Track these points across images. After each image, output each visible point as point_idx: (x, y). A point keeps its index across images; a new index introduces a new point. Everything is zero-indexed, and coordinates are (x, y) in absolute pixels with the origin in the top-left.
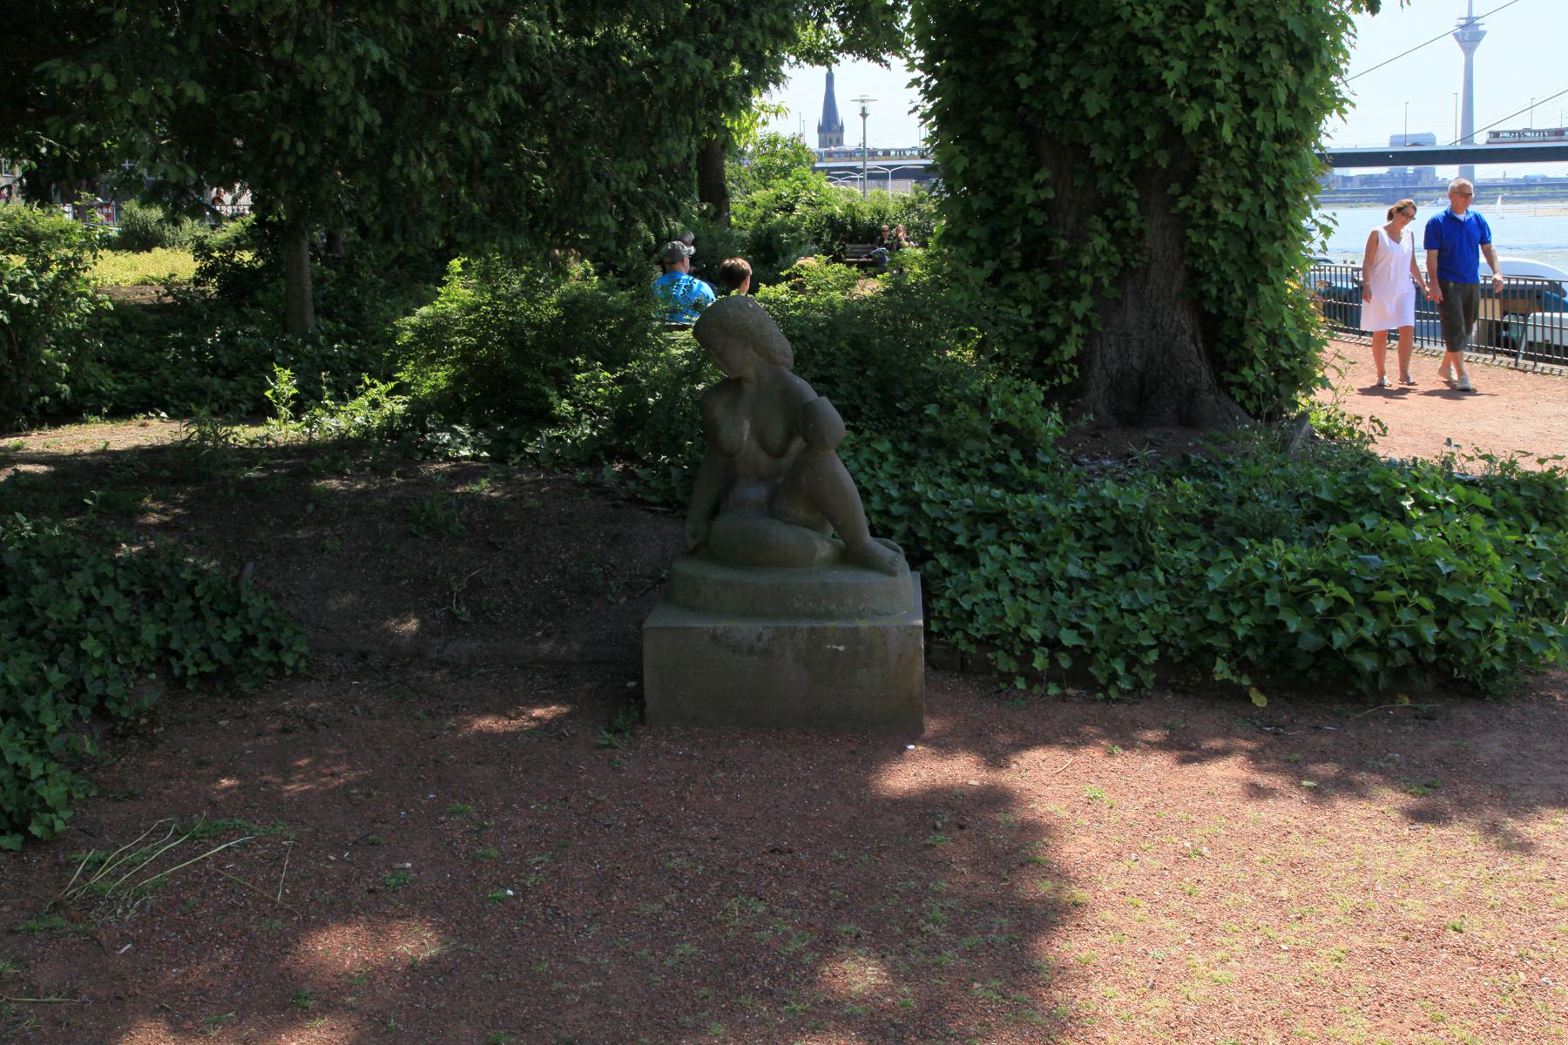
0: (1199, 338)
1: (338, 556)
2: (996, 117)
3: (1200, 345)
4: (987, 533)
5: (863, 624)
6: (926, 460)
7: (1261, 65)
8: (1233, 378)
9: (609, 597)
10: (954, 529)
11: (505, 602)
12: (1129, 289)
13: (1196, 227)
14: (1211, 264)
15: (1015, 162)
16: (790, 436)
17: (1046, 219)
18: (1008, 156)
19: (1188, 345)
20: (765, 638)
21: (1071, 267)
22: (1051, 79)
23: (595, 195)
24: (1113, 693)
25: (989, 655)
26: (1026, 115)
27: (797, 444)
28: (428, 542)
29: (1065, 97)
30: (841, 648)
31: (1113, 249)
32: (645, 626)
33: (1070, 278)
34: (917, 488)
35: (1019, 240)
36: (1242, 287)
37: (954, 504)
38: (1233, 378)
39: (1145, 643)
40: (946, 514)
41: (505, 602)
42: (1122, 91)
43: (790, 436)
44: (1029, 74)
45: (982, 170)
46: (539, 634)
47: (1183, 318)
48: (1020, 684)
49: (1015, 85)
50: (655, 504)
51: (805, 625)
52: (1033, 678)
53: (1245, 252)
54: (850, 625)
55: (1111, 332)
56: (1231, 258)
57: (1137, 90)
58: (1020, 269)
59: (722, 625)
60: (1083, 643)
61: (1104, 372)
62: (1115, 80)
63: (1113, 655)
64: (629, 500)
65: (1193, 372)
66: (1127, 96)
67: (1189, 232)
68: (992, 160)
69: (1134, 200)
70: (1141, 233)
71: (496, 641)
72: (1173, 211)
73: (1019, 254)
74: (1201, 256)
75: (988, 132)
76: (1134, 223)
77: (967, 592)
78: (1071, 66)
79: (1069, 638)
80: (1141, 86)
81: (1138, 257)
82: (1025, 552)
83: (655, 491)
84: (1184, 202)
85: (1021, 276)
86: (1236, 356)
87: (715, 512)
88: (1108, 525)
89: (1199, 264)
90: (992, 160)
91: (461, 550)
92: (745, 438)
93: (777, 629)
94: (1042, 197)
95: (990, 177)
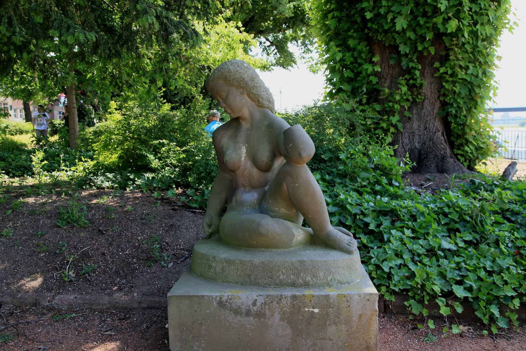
0: (445, 133)
1: (9, 239)
2: (355, 35)
3: (445, 137)
4: (386, 222)
5: (332, 292)
6: (339, 184)
7: (480, 4)
8: (460, 152)
9: (163, 263)
10: (367, 220)
11: (99, 267)
12: (414, 112)
13: (447, 82)
14: (452, 99)
15: (363, 55)
16: (274, 156)
17: (378, 81)
18: (360, 52)
19: (440, 137)
20: (258, 304)
21: (390, 101)
22: (382, 13)
23: (145, 5)
24: (495, 331)
25: (405, 303)
26: (369, 33)
27: (280, 162)
28: (65, 230)
29: (389, 20)
30: (316, 311)
31: (409, 93)
32: (169, 294)
33: (390, 107)
34: (342, 197)
35: (365, 91)
36: (466, 110)
37: (365, 205)
38: (460, 152)
39: (509, 294)
40: (362, 211)
41: (99, 267)
42: (415, 18)
43: (274, 156)
44: (371, 12)
45: (349, 59)
46: (116, 288)
47: (438, 125)
48: (431, 324)
49: (363, 18)
50: (196, 208)
51: (288, 292)
52: (438, 319)
53: (468, 93)
54: (323, 293)
55: (406, 132)
56: (461, 96)
57: (422, 17)
58: (366, 104)
59: (226, 293)
60: (469, 295)
61: (403, 150)
62: (412, 12)
63: (489, 303)
64: (183, 206)
65: (443, 149)
66: (418, 19)
67: (444, 84)
68: (353, 55)
69: (418, 70)
70: (421, 85)
71: (87, 293)
72: (436, 75)
73: (366, 96)
74: (448, 96)
75: (351, 43)
76: (419, 81)
77: (385, 260)
78: (391, 6)
79: (460, 292)
80: (425, 14)
81: (419, 97)
82: (413, 233)
83: (196, 201)
84: (442, 70)
85: (366, 107)
86: (461, 142)
87: (223, 211)
88: (455, 216)
89: (447, 100)
90: (353, 55)
91: (82, 234)
92: (243, 159)
93: (268, 296)
94: (376, 70)
95: (352, 63)
